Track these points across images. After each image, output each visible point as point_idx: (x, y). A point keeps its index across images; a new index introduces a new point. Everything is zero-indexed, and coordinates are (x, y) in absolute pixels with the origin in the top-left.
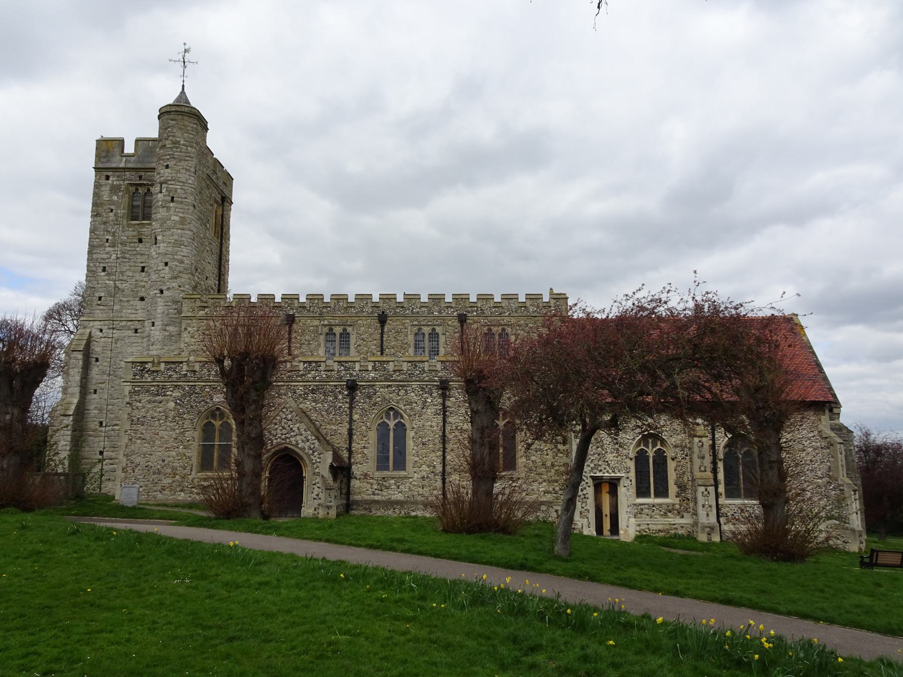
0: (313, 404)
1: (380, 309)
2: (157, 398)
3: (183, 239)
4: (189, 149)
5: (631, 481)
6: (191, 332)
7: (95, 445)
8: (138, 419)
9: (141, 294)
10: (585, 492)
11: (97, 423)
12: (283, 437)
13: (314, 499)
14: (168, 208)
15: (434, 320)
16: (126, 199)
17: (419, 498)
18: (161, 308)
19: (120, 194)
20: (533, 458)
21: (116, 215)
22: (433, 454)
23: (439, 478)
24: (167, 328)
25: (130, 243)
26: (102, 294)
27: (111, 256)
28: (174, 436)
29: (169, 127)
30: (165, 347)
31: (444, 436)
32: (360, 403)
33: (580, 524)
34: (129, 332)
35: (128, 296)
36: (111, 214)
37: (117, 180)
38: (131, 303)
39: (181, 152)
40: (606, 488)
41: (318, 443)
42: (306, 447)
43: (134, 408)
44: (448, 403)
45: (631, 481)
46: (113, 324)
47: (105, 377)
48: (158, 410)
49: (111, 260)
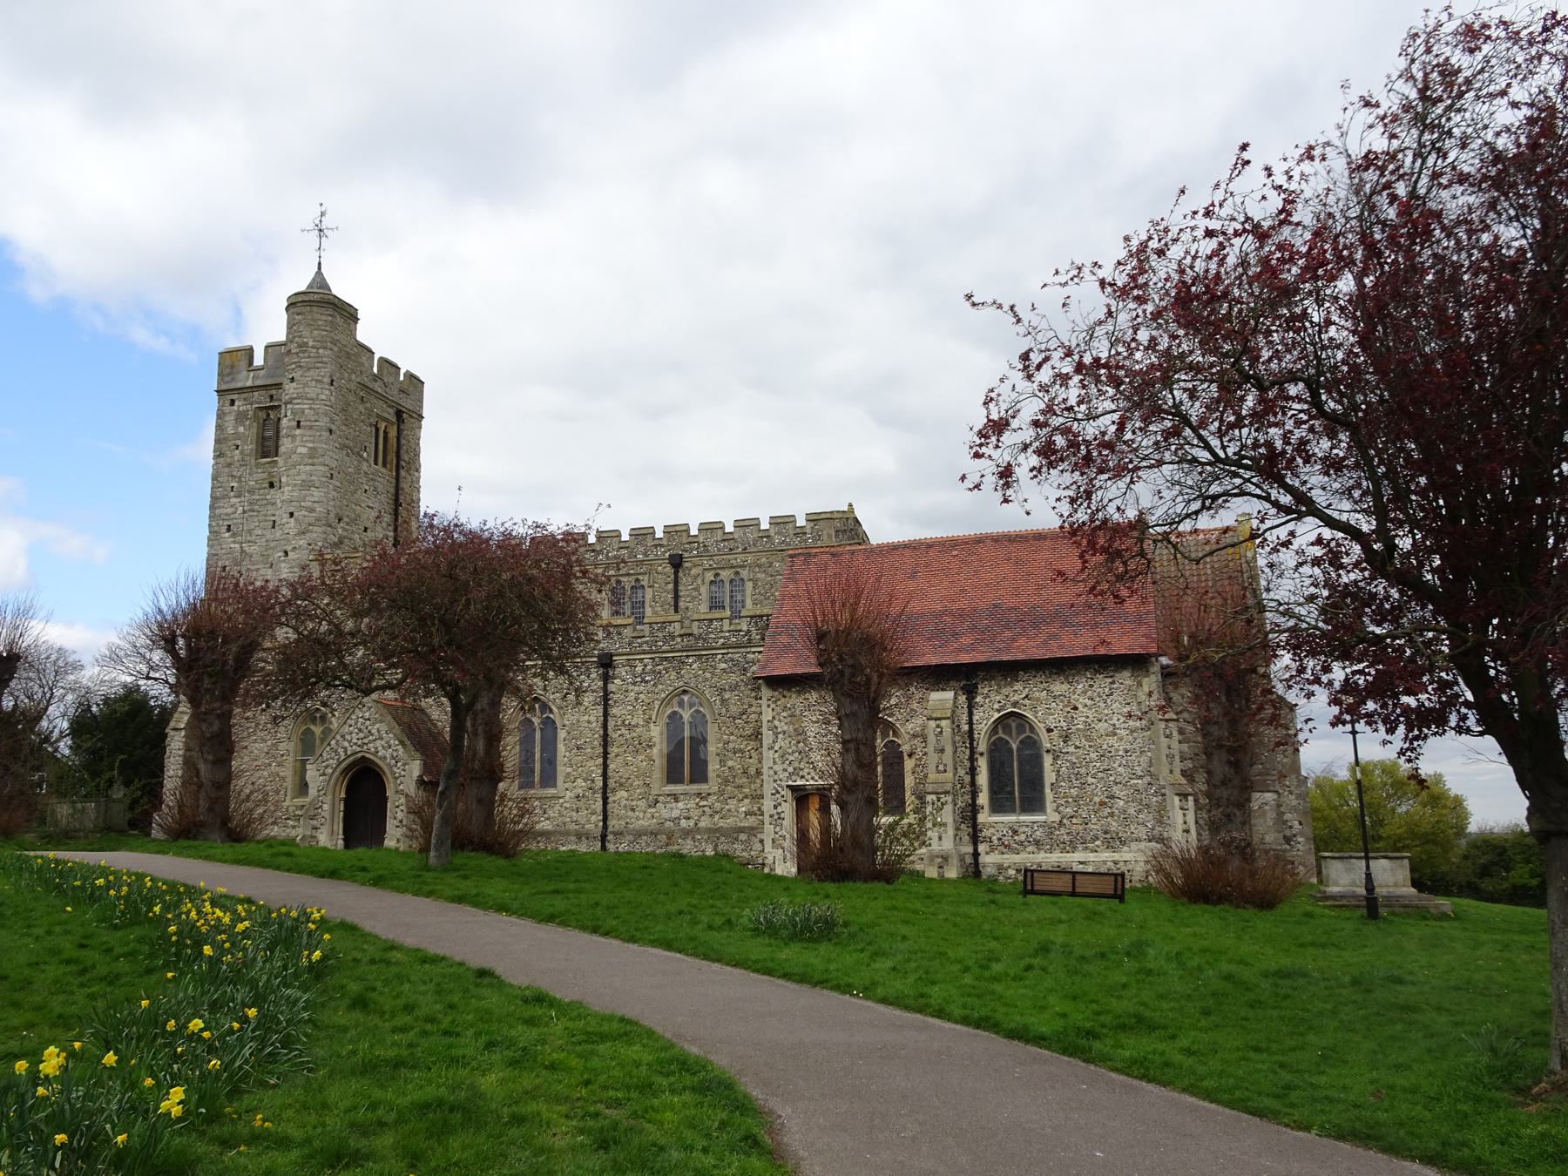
4: (321, 351)
10: (779, 809)
12: (360, 742)
14: (294, 437)
17: (572, 827)
20: (730, 763)
21: (241, 453)
22: (591, 763)
23: (599, 796)
28: (266, 750)
31: (605, 736)
33: (770, 858)
40: (814, 804)
44: (611, 687)
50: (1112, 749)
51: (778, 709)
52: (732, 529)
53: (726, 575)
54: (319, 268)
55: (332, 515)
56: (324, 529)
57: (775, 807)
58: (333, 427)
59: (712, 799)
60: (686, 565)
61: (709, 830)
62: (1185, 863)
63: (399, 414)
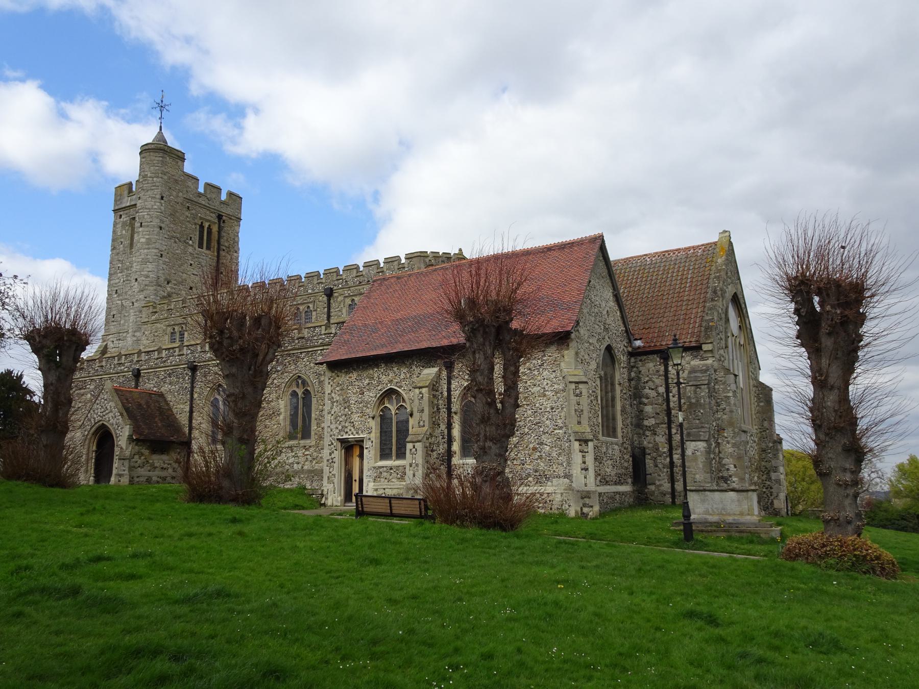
3: (149, 257)
4: (155, 179)
5: (372, 442)
15: (308, 297)
26: (115, 313)
33: (325, 490)
39: (148, 183)
45: (372, 442)
50: (542, 407)
51: (334, 385)
54: (161, 129)
55: (162, 279)
56: (154, 287)
57: (330, 454)
58: (163, 225)
59: (312, 450)
60: (335, 295)
61: (309, 471)
63: (220, 217)
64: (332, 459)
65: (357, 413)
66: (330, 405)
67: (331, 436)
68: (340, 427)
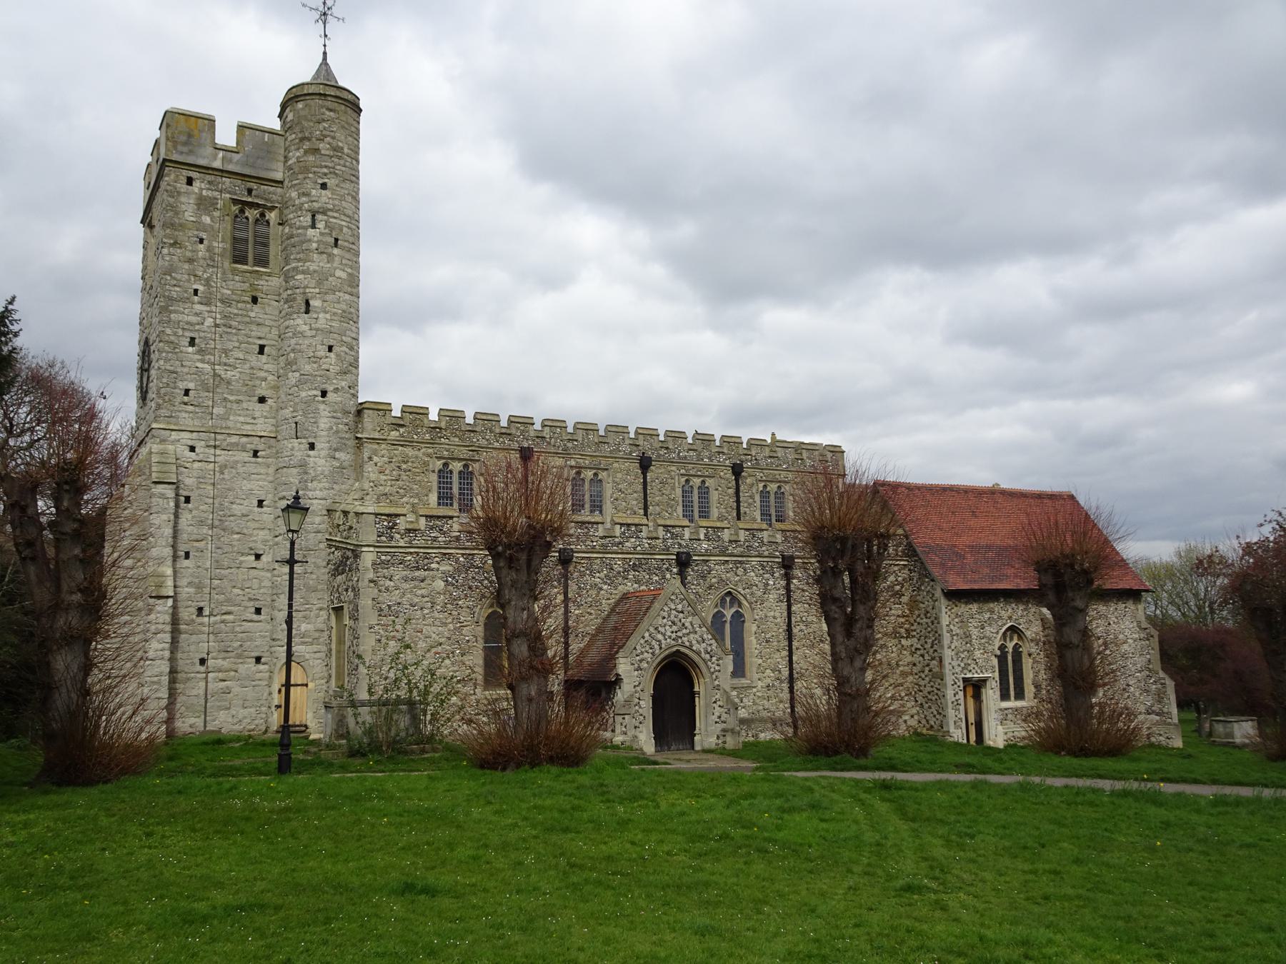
0: (636, 586)
1: (641, 448)
2: (417, 573)
6: (379, 464)
7: (193, 648)
8: (389, 607)
9: (261, 392)
11: (194, 610)
13: (716, 722)
16: (228, 225)
17: (765, 714)
18: (326, 420)
19: (217, 214)
21: (209, 249)
22: (777, 655)
23: (785, 686)
24: (337, 455)
25: (238, 302)
26: (191, 386)
27: (204, 319)
28: (446, 634)
29: (324, 120)
30: (335, 486)
32: (693, 584)
34: (244, 454)
35: (239, 392)
36: (202, 246)
37: (209, 189)
38: (245, 405)
39: (345, 166)
40: (970, 691)
41: (716, 644)
42: (702, 650)
43: (383, 589)
46: (215, 440)
47: (205, 530)
48: (419, 592)
49: (204, 327)
51: (953, 616)
52: (472, 422)
53: (773, 487)
57: (955, 696)
62: (813, 719)
64: (957, 700)
65: (979, 649)
66: (950, 639)
67: (953, 674)
68: (962, 665)
